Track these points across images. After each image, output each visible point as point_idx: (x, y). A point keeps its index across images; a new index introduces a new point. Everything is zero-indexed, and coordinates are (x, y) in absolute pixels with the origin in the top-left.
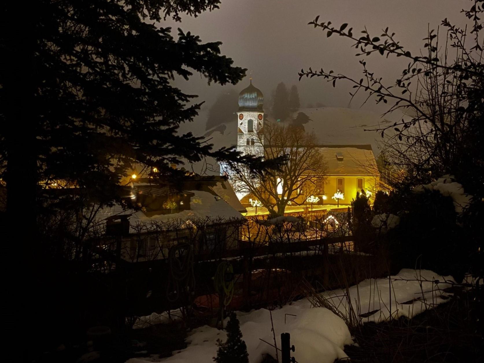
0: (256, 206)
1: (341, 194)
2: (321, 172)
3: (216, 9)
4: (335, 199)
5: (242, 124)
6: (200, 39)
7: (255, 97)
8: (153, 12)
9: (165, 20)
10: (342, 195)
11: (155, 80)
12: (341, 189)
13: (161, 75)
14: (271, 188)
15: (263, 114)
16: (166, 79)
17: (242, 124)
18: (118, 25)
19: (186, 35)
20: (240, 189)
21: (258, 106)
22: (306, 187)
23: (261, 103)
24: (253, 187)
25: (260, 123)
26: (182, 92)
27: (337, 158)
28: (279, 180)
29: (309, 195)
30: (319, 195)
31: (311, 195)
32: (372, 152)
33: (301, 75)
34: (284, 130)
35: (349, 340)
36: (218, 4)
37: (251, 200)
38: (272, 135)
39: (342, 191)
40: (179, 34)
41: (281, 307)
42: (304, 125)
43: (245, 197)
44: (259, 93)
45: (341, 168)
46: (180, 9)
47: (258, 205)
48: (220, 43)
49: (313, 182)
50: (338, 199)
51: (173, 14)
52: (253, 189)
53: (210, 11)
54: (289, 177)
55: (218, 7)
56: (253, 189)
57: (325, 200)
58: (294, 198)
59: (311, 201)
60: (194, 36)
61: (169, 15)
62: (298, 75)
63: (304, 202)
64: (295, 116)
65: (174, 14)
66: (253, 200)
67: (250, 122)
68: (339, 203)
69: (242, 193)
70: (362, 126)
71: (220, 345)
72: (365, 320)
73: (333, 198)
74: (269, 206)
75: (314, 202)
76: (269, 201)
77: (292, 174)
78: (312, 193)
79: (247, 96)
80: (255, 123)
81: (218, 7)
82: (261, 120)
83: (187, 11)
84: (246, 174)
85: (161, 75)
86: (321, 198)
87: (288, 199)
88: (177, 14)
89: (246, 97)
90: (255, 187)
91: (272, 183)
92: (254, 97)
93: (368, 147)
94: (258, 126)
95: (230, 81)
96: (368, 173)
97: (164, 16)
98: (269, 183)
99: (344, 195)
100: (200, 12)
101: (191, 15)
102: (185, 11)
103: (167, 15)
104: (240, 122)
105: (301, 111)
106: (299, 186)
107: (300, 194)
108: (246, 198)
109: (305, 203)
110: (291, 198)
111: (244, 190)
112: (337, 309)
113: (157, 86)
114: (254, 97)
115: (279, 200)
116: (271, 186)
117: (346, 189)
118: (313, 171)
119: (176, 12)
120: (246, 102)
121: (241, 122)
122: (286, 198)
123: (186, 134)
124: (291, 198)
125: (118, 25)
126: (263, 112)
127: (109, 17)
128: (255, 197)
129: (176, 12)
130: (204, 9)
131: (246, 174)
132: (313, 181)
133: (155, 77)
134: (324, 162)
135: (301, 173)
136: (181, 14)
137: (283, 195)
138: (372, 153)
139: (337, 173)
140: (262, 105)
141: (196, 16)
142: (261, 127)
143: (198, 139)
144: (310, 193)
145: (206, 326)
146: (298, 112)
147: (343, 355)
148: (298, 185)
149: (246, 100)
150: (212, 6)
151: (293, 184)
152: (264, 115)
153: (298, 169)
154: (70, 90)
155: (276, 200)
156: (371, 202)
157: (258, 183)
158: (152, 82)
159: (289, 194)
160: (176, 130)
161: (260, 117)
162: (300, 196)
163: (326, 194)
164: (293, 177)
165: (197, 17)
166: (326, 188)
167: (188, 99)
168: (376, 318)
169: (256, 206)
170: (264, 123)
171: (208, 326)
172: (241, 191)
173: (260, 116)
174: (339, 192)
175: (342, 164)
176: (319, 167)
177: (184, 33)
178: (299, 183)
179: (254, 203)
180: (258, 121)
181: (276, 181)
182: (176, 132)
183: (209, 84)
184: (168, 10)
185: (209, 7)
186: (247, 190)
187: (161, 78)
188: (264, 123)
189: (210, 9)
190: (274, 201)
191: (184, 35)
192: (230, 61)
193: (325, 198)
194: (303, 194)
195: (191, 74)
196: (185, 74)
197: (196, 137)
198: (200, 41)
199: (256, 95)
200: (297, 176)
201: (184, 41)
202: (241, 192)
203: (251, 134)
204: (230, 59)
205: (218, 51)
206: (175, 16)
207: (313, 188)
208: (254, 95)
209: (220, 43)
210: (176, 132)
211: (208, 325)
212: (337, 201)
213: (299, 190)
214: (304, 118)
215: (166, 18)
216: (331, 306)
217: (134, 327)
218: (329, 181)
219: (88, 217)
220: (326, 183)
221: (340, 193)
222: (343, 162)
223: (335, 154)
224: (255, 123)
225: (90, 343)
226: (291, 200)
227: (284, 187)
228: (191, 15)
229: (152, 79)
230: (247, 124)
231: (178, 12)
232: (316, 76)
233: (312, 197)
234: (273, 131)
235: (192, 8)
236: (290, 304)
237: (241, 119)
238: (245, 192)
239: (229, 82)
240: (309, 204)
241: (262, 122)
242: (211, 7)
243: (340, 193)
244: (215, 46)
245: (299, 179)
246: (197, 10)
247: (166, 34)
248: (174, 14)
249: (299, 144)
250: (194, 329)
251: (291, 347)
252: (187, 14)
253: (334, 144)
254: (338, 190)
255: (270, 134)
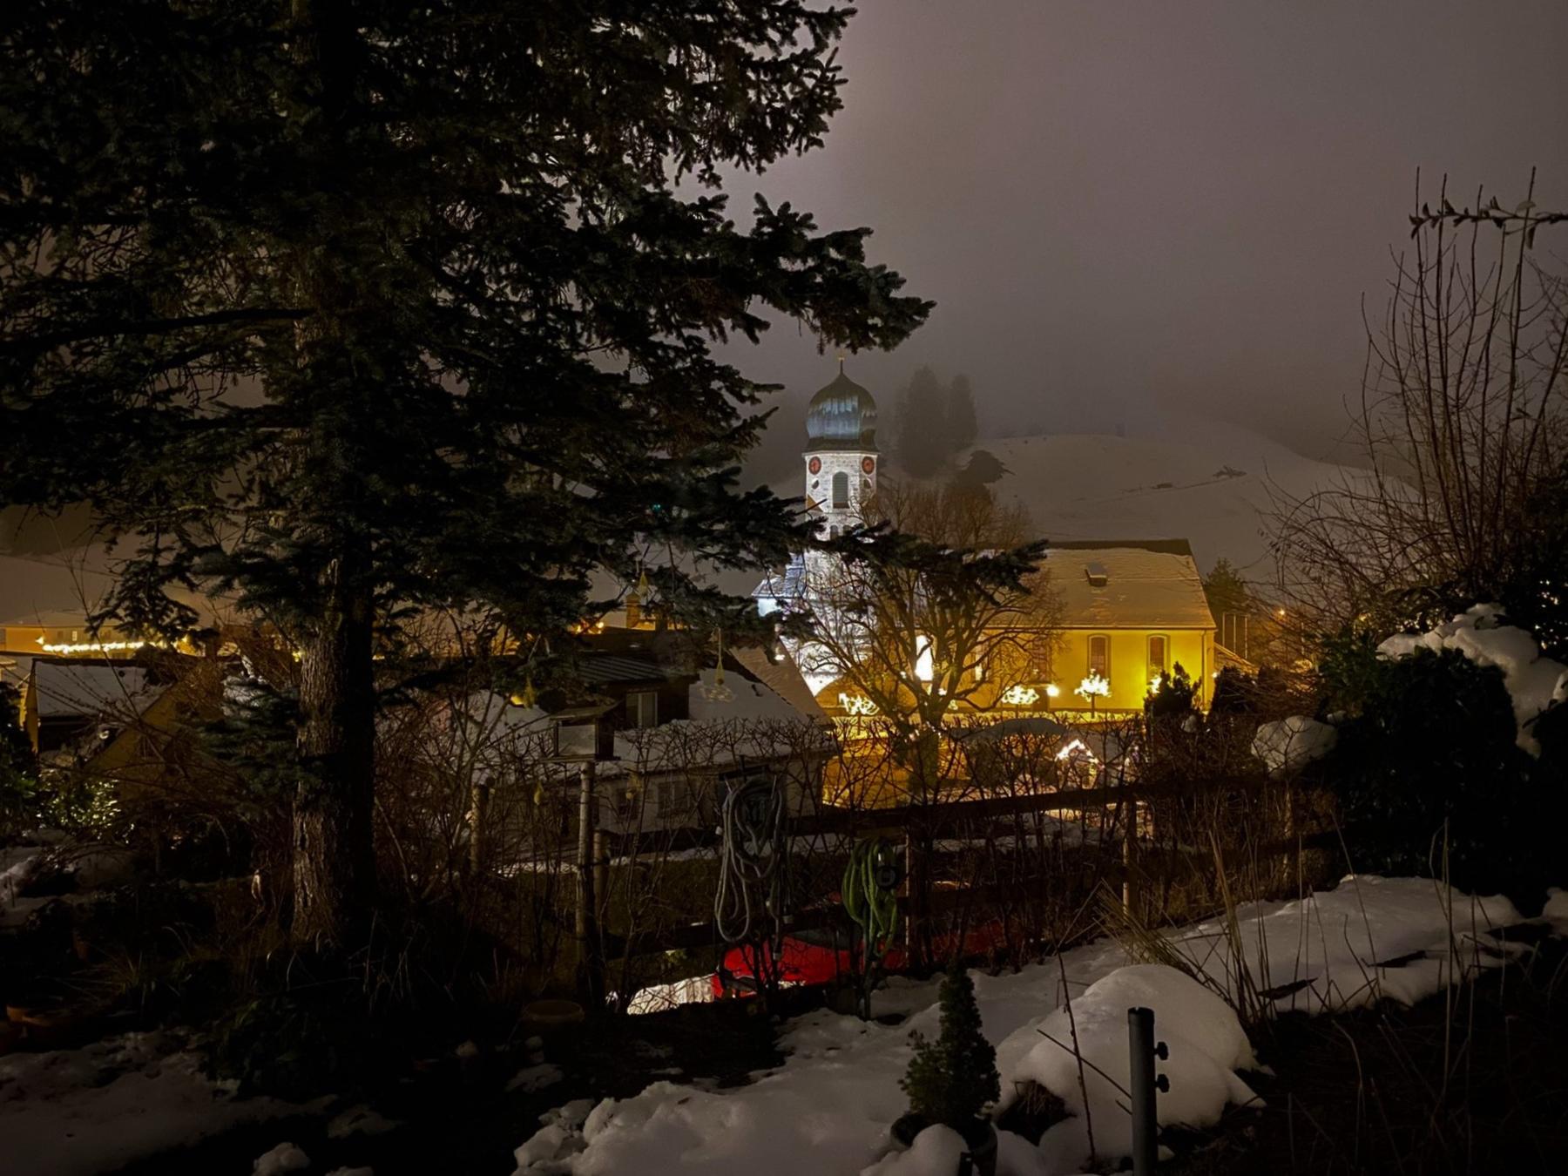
0: (859, 714)
1: (1101, 680)
2: (1045, 617)
3: (815, 147)
4: (1083, 694)
5: (816, 485)
6: (813, 222)
7: (853, 408)
8: (646, 165)
9: (677, 183)
10: (1105, 682)
11: (669, 347)
12: (1101, 667)
13: (686, 332)
14: (901, 663)
15: (874, 457)
16: (701, 341)
17: (816, 485)
18: (551, 203)
19: (775, 214)
20: (815, 665)
21: (862, 435)
22: (1001, 659)
23: (871, 427)
24: (851, 659)
25: (866, 482)
26: (743, 375)
27: (1090, 579)
28: (921, 641)
29: (1012, 683)
30: (1038, 683)
31: (1017, 684)
32: (1191, 560)
33: (1417, 222)
34: (939, 501)
35: (1248, 1059)
36: (821, 136)
37: (843, 696)
38: (903, 512)
39: (1103, 673)
40: (757, 212)
41: (1017, 970)
42: (988, 486)
43: (828, 689)
44: (865, 399)
45: (1102, 606)
46: (717, 151)
47: (864, 711)
48: (868, 232)
49: (1022, 647)
50: (1093, 695)
51: (699, 166)
52: (850, 665)
53: (799, 154)
54: (950, 632)
55: (820, 143)
56: (850, 665)
57: (1054, 698)
58: (967, 692)
59: (1015, 701)
60: (796, 215)
61: (690, 171)
62: (1409, 222)
63: (995, 703)
64: (964, 460)
65: (703, 166)
66: (848, 696)
67: (840, 481)
68: (1096, 706)
69: (819, 678)
70: (1159, 487)
71: (918, 1046)
72: (1283, 1004)
73: (1076, 691)
74: (896, 713)
75: (1024, 702)
76: (896, 700)
77: (962, 623)
78: (1018, 677)
79: (830, 406)
80: (854, 481)
81: (820, 143)
82: (868, 473)
83: (736, 158)
84: (832, 624)
85: (686, 332)
86: (1042, 693)
87: (951, 695)
88: (710, 167)
89: (828, 409)
90: (856, 660)
91: (905, 649)
92: (850, 410)
93: (1180, 547)
94: (863, 491)
95: (877, 340)
96: (1177, 620)
97: (676, 173)
98: (897, 649)
99: (1109, 684)
100: (770, 161)
101: (747, 168)
102: (731, 158)
103: (685, 170)
104: (811, 479)
105: (981, 448)
106: (981, 660)
107: (983, 680)
108: (831, 690)
109: (998, 705)
110: (959, 689)
111: (827, 668)
112: (1200, 969)
113: (673, 362)
114: (850, 410)
115: (926, 697)
116: (903, 655)
117: (1116, 664)
118: (1023, 616)
119: (707, 161)
120: (828, 425)
121: (814, 481)
122: (942, 692)
123: (753, 491)
124: (959, 689)
125: (551, 203)
126: (874, 450)
127: (540, 177)
128: (855, 688)
129: (707, 161)
130: (784, 151)
131: (832, 624)
132: (1022, 643)
133: (672, 340)
134: (1055, 590)
135: (986, 621)
136: (719, 166)
137: (936, 683)
138: (1192, 564)
139: (1091, 621)
140: (873, 432)
141: (760, 170)
142: (870, 494)
143: (788, 502)
144: (1012, 676)
145: (824, 1010)
146: (972, 450)
147: (1244, 1093)
148: (978, 657)
149: (829, 417)
150: (804, 142)
151: (964, 650)
152: (878, 459)
153: (978, 608)
154: (436, 380)
155: (917, 696)
156: (1206, 694)
157: (866, 649)
158: (660, 352)
159: (953, 683)
160: (734, 478)
161: (866, 465)
162: (984, 686)
163: (1059, 682)
164: (964, 631)
165: (763, 174)
166: (1058, 662)
167: (757, 395)
168: (1308, 1002)
169: (859, 714)
170: (878, 481)
171: (830, 1012)
172: (819, 670)
173: (867, 468)
174: (1095, 675)
175: (1103, 595)
176: (1039, 605)
177: (770, 206)
178: (978, 648)
179: (853, 704)
180: (861, 476)
181: (914, 646)
182: (736, 483)
183: (821, 351)
184: (686, 158)
185: (797, 145)
186: (835, 670)
187: (688, 340)
188: (879, 484)
189: (799, 149)
190: (911, 700)
191: (770, 212)
192: (893, 281)
193: (1053, 691)
194: (991, 682)
195: (765, 325)
196: (752, 326)
197: (782, 498)
198: (813, 227)
199: (856, 404)
200: (977, 628)
201: (766, 230)
202: (815, 675)
203: (845, 514)
204: (895, 274)
205: (857, 253)
206: (704, 171)
207: (1022, 663)
208: (850, 405)
209: (868, 232)
210: (736, 483)
211: (831, 1008)
212: (1089, 700)
213: (978, 671)
214: (990, 468)
215: (680, 180)
216: (1185, 961)
217: (630, 1010)
218: (1069, 642)
219: (479, 719)
220: (1060, 648)
221: (1098, 677)
222: (1105, 590)
223: (1084, 567)
224: (854, 481)
225: (535, 1041)
226: (959, 697)
227: (937, 660)
228: (747, 168)
229: (661, 343)
230: (831, 486)
231: (713, 162)
232: (1467, 222)
233: (1018, 690)
234: (907, 503)
235: (750, 149)
236: (1041, 963)
237: (815, 472)
238: (827, 673)
239: (875, 344)
240: (1008, 710)
241: (872, 479)
242: (800, 144)
243: (1098, 677)
244: (849, 241)
245: (980, 639)
246: (765, 153)
247: (712, 215)
248: (703, 166)
249: (982, 539)
250: (792, 1020)
251: (1156, 1046)
252: (737, 165)
253: (1096, 539)
254: (1093, 670)
255: (898, 513)
